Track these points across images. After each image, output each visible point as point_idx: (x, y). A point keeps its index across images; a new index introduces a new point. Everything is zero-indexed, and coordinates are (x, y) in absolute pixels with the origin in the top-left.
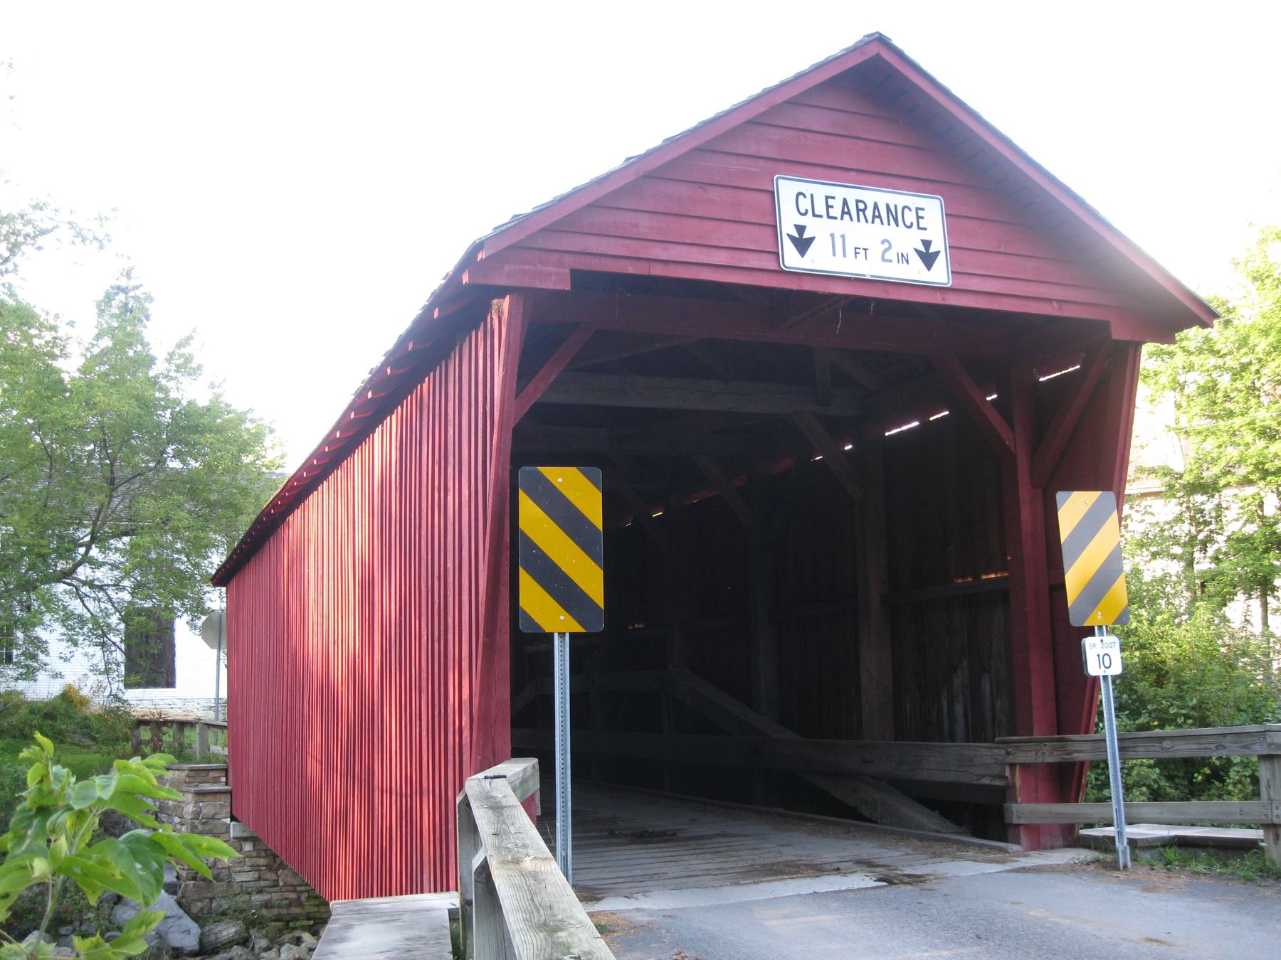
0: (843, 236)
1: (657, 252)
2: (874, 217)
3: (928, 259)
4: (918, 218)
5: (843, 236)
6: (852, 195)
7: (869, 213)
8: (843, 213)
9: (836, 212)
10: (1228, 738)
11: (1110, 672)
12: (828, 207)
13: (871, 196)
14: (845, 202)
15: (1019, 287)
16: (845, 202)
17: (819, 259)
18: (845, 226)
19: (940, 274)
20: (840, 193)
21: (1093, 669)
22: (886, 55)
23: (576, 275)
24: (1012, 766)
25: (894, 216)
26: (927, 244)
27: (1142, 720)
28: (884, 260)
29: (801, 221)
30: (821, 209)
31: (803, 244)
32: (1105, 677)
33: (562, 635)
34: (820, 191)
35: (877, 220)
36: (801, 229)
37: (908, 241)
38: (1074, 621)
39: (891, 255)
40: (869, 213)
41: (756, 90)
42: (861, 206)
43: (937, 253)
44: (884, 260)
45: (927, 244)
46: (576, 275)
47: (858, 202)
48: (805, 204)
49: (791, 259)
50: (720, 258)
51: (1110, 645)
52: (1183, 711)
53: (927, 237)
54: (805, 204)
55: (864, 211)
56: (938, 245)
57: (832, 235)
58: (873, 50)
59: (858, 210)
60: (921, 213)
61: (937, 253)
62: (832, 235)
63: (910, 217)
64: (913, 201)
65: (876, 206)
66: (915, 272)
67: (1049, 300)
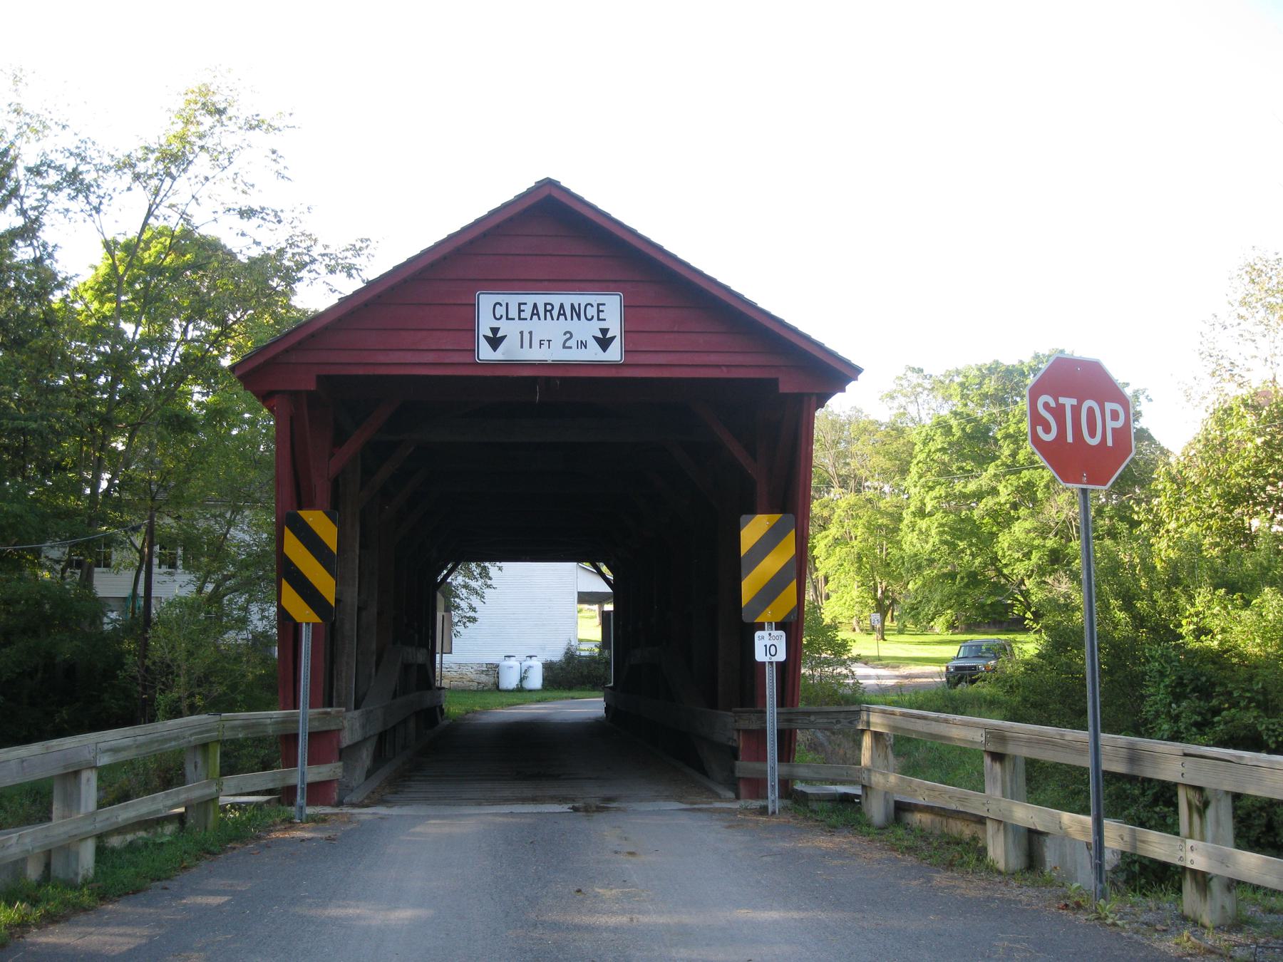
0: (531, 333)
1: (382, 358)
2: (559, 314)
3: (604, 342)
4: (599, 311)
5: (531, 333)
6: (541, 300)
7: (555, 313)
8: (533, 314)
9: (527, 314)
10: (843, 715)
11: (774, 659)
12: (520, 311)
13: (568, 300)
14: (535, 306)
15: (696, 356)
16: (535, 306)
17: (509, 351)
18: (526, 326)
19: (614, 353)
20: (530, 299)
21: (760, 656)
22: (556, 194)
23: (320, 379)
24: (738, 731)
25: (577, 312)
26: (604, 331)
27: (1215, 702)
28: (564, 347)
29: (496, 324)
30: (513, 312)
31: (495, 342)
32: (771, 663)
33: (308, 624)
34: (513, 300)
35: (562, 318)
36: (495, 330)
37: (587, 330)
38: (746, 618)
39: (572, 343)
40: (555, 313)
41: (442, 235)
42: (549, 307)
43: (613, 338)
44: (564, 347)
45: (604, 331)
46: (320, 379)
47: (546, 305)
48: (500, 311)
49: (486, 353)
50: (430, 357)
51: (777, 638)
52: (1248, 695)
53: (603, 325)
54: (500, 311)
55: (550, 311)
56: (615, 330)
57: (522, 333)
58: (545, 192)
59: (546, 311)
60: (601, 308)
61: (613, 338)
62: (522, 333)
63: (592, 312)
64: (595, 299)
65: (562, 306)
66: (593, 353)
67: (718, 366)
